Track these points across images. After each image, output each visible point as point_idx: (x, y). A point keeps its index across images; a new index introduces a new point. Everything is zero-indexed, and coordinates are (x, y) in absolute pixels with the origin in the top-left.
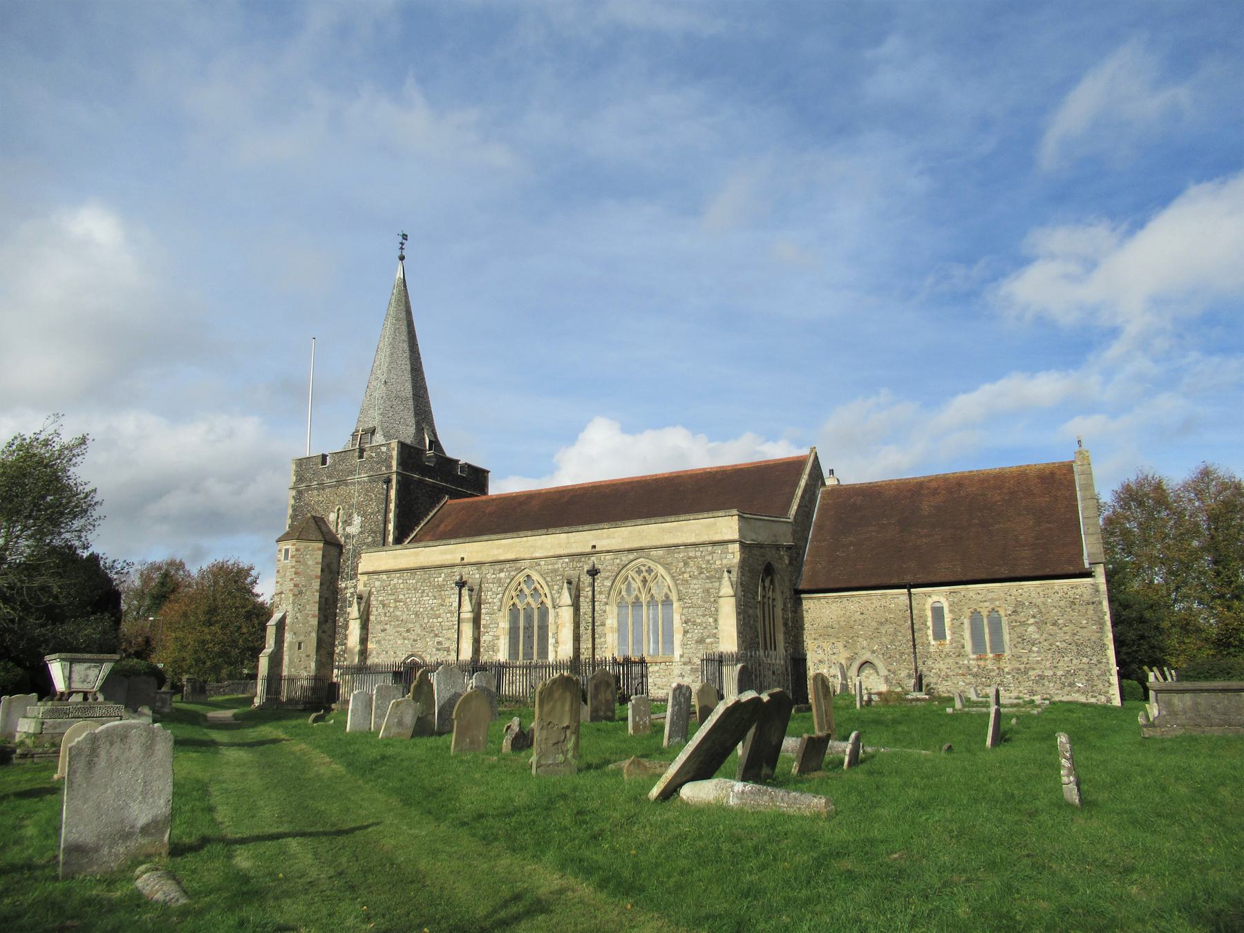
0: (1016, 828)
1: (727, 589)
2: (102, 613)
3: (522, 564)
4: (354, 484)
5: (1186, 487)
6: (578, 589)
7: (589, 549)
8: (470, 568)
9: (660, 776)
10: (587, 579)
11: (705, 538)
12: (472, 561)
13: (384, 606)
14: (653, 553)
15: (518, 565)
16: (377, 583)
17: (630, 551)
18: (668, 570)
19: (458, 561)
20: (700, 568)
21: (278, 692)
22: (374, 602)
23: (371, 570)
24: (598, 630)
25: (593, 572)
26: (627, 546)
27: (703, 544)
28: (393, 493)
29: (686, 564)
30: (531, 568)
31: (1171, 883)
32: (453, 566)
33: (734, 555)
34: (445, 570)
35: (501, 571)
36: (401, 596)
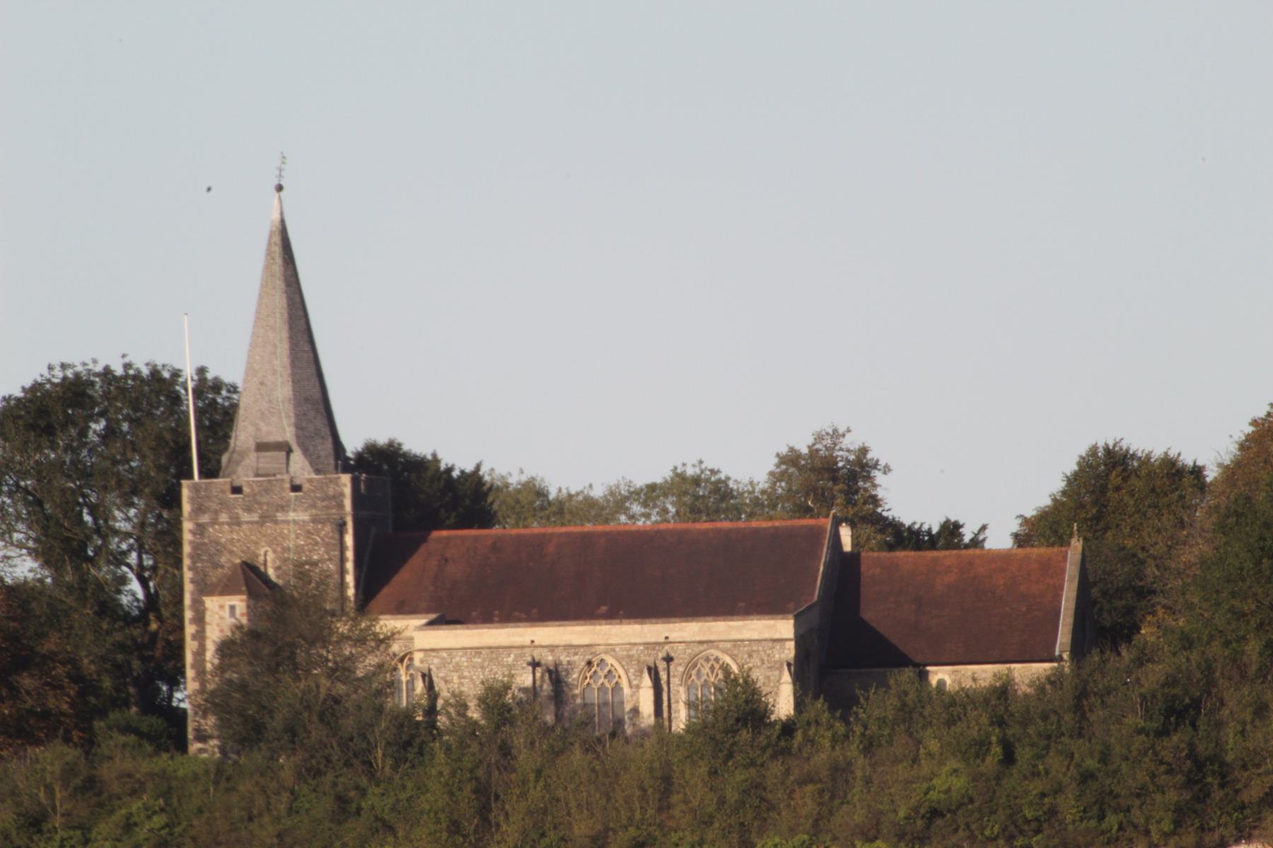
0: (280, 539)
1: (787, 677)
2: (65, 378)
3: (599, 649)
4: (287, 522)
5: (1043, 529)
6: (657, 673)
7: (662, 640)
8: (540, 650)
9: (477, 650)
10: (662, 665)
11: (767, 636)
12: (544, 643)
13: (446, 682)
14: (721, 645)
15: (593, 650)
16: (436, 661)
17: (701, 643)
18: (734, 660)
19: (528, 643)
20: (762, 661)
21: (414, 690)
22: (435, 679)
23: (427, 647)
24: (673, 706)
25: (669, 659)
26: (698, 639)
27: (766, 640)
28: (349, 540)
29: (750, 656)
30: (606, 652)
31: (249, 510)
32: (523, 647)
33: (789, 651)
34: (515, 651)
35: (576, 654)
36: (466, 674)
